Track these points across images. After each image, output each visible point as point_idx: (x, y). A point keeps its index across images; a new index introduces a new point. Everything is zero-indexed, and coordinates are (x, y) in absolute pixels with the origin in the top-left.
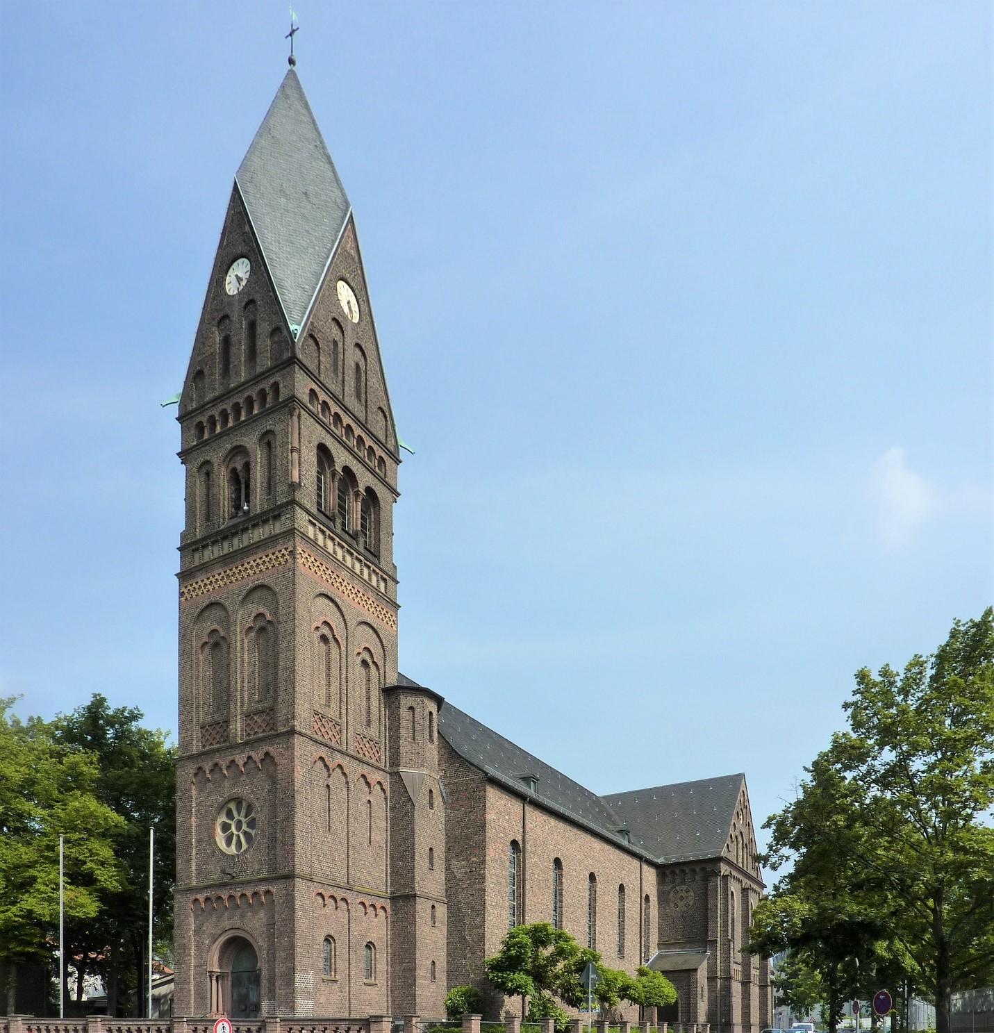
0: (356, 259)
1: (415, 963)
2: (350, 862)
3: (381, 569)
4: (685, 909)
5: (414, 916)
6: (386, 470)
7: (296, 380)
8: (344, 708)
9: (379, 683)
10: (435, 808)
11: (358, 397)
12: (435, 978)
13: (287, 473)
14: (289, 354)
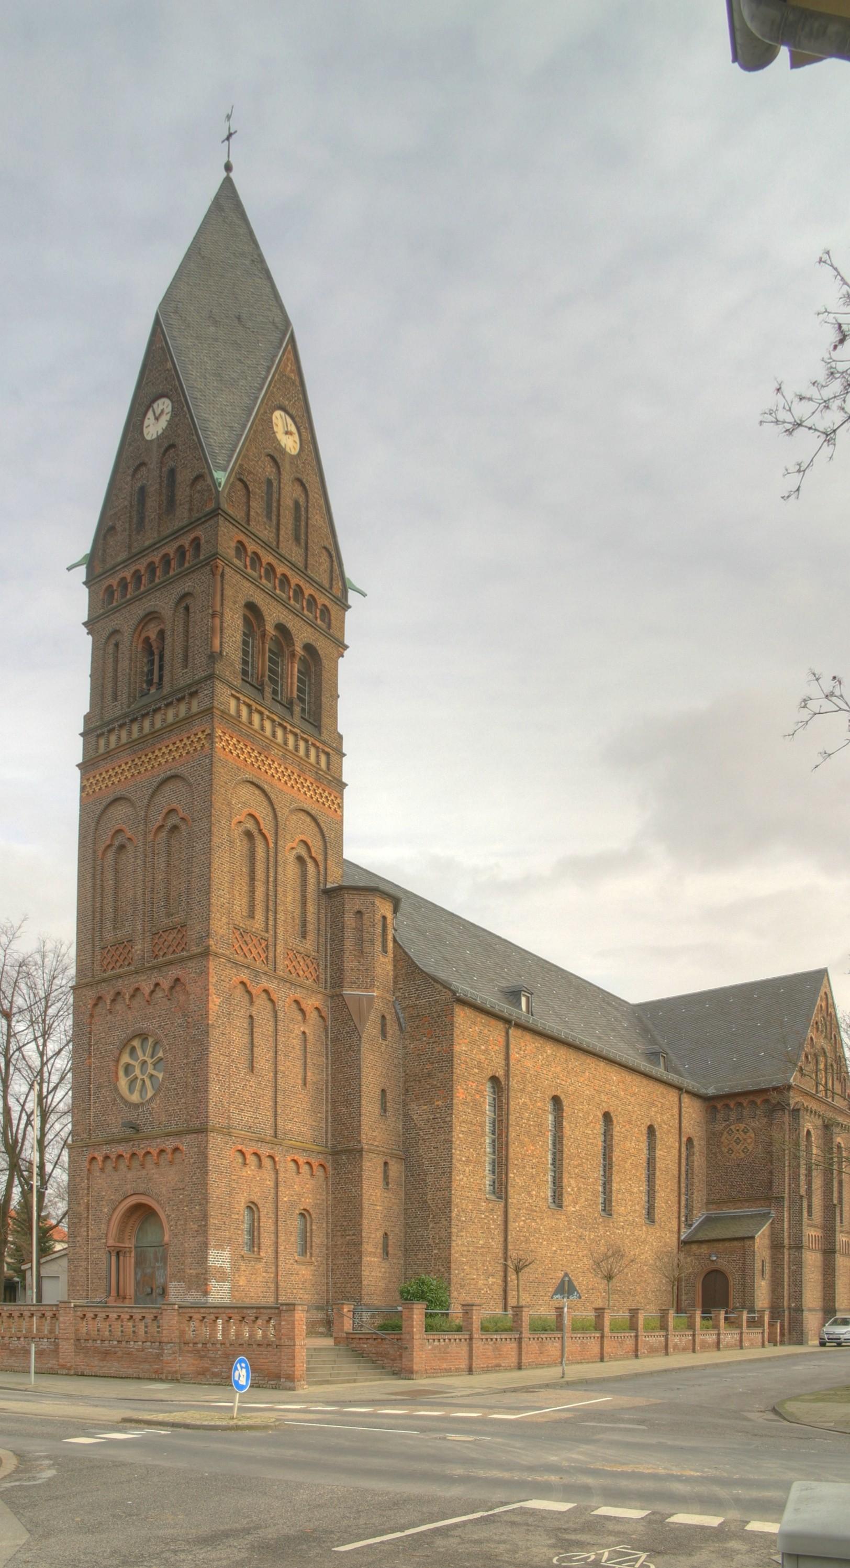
0: (297, 383)
1: (361, 1237)
2: (279, 1111)
3: (324, 743)
4: (743, 1155)
5: (360, 1176)
6: (330, 620)
7: (220, 533)
8: (271, 918)
9: (319, 883)
10: (390, 1039)
11: (297, 539)
12: (387, 1254)
13: (209, 641)
14: (213, 505)
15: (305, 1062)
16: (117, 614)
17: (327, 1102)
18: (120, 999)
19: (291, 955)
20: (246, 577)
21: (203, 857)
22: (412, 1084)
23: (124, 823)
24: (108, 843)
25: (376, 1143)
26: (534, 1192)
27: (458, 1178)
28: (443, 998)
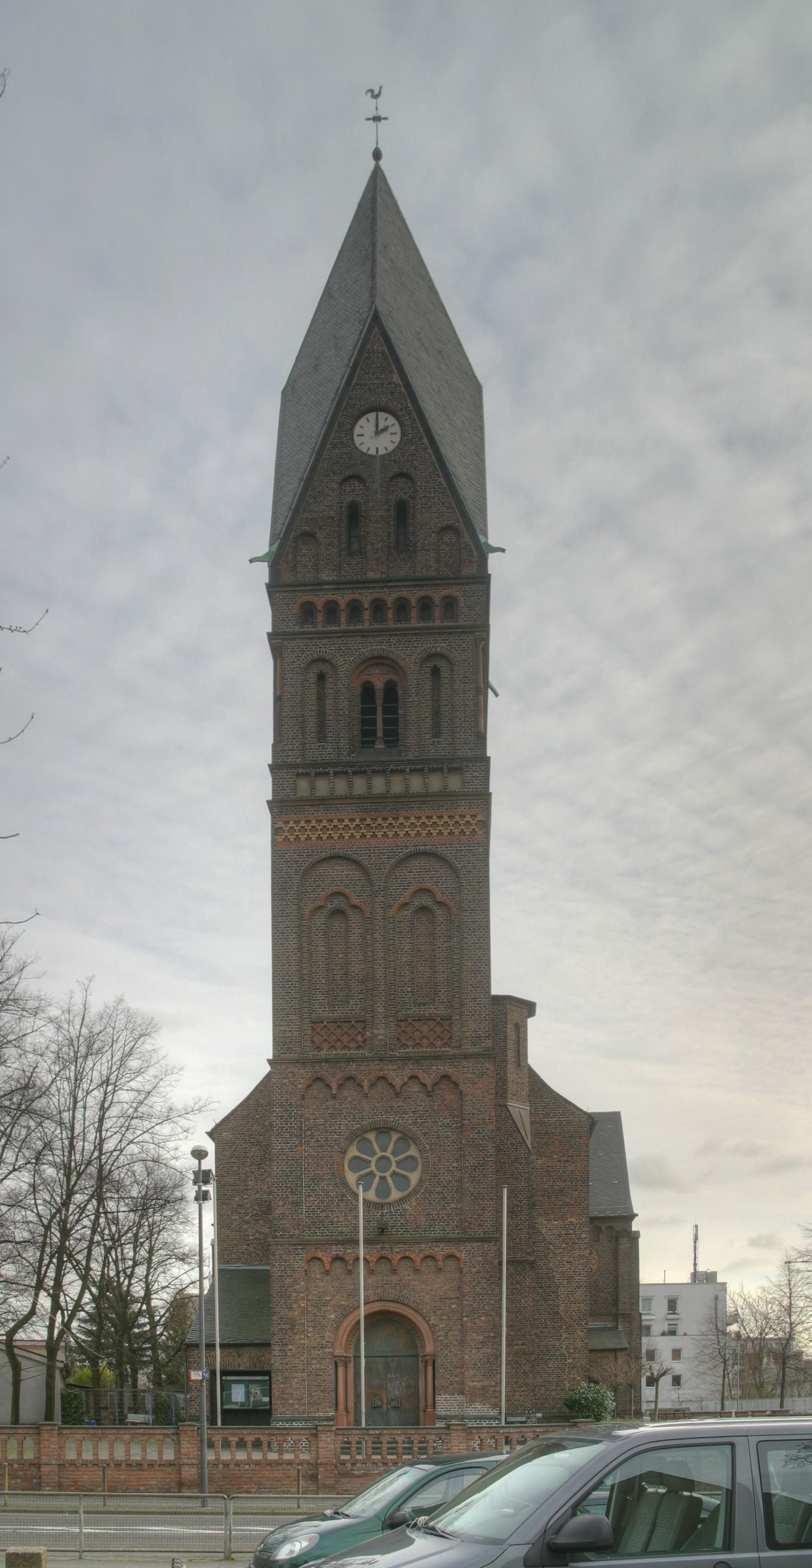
16: (325, 641)
24: (319, 903)
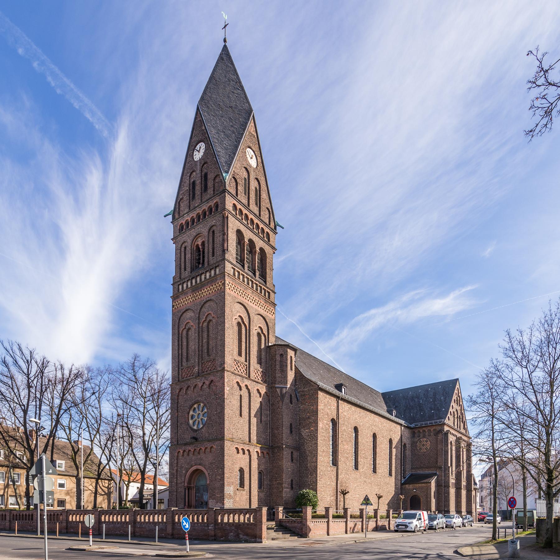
3: (268, 288)
4: (425, 451)
10: (293, 404)
15: (261, 413)
17: (270, 428)
18: (189, 388)
19: (256, 372)
20: (237, 219)
21: (222, 332)
22: (302, 421)
23: (190, 319)
25: (288, 444)
26: (348, 464)
27: (320, 458)
28: (314, 388)
